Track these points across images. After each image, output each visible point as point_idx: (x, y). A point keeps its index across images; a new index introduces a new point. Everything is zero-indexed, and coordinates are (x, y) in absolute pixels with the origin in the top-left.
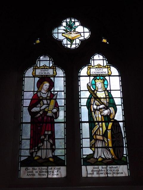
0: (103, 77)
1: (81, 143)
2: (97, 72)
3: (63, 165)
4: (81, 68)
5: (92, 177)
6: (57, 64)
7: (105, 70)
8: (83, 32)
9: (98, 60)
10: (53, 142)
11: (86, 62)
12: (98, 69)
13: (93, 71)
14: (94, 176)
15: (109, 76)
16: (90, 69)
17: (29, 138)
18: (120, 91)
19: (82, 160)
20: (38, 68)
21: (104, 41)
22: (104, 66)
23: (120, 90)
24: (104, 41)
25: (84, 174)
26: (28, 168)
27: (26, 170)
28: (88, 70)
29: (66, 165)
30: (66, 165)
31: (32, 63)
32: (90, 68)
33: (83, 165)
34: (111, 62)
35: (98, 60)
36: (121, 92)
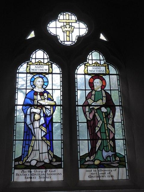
0: (42, 75)
1: (62, 143)
2: (40, 70)
3: (61, 168)
4: (20, 64)
5: (103, 180)
6: (53, 59)
7: (46, 67)
8: (55, 27)
9: (94, 56)
10: (50, 144)
11: (83, 60)
12: (39, 66)
13: (90, 69)
14: (104, 179)
15: (52, 73)
16: (30, 66)
17: (116, 140)
18: (60, 90)
19: (63, 160)
20: (33, 64)
21: (102, 37)
22: (44, 63)
23: (60, 89)
24: (102, 37)
25: (81, 178)
26: (24, 171)
27: (22, 172)
28: (85, 68)
29: (63, 167)
30: (63, 167)
31: (26, 58)
32: (87, 66)
33: (81, 168)
34: (109, 60)
35: (94, 56)
36: (61, 91)
